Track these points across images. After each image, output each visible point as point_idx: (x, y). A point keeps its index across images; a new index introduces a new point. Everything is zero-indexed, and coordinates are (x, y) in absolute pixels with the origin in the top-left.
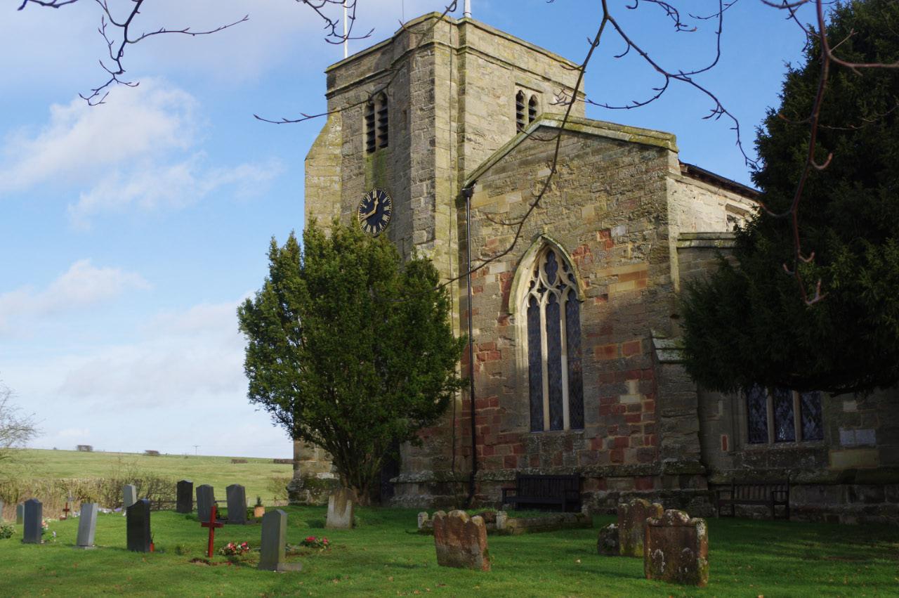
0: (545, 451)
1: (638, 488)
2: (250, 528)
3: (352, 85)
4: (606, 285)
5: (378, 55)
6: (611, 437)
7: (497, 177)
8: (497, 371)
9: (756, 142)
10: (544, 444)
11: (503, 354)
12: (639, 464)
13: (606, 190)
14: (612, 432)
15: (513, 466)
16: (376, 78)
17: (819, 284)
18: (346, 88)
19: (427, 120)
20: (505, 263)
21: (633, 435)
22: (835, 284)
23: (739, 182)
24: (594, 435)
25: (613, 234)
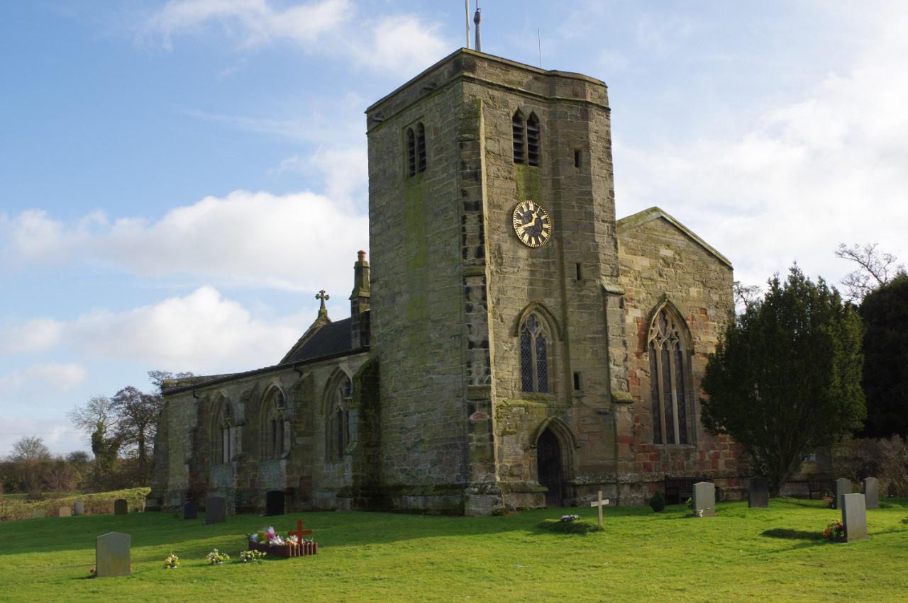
0: (672, 459)
1: (730, 485)
2: (355, 547)
3: (500, 86)
4: (706, 347)
5: (531, 77)
6: (712, 452)
7: (631, 240)
8: (637, 394)
9: (796, 279)
10: (672, 454)
11: (641, 382)
12: (728, 470)
13: (702, 282)
14: (713, 448)
15: (650, 470)
16: (528, 96)
17: (567, 516)
18: (492, 84)
19: (605, 171)
20: (639, 310)
21: (723, 451)
22: (723, 428)
23: (244, 371)
24: (702, 449)
25: (708, 313)
